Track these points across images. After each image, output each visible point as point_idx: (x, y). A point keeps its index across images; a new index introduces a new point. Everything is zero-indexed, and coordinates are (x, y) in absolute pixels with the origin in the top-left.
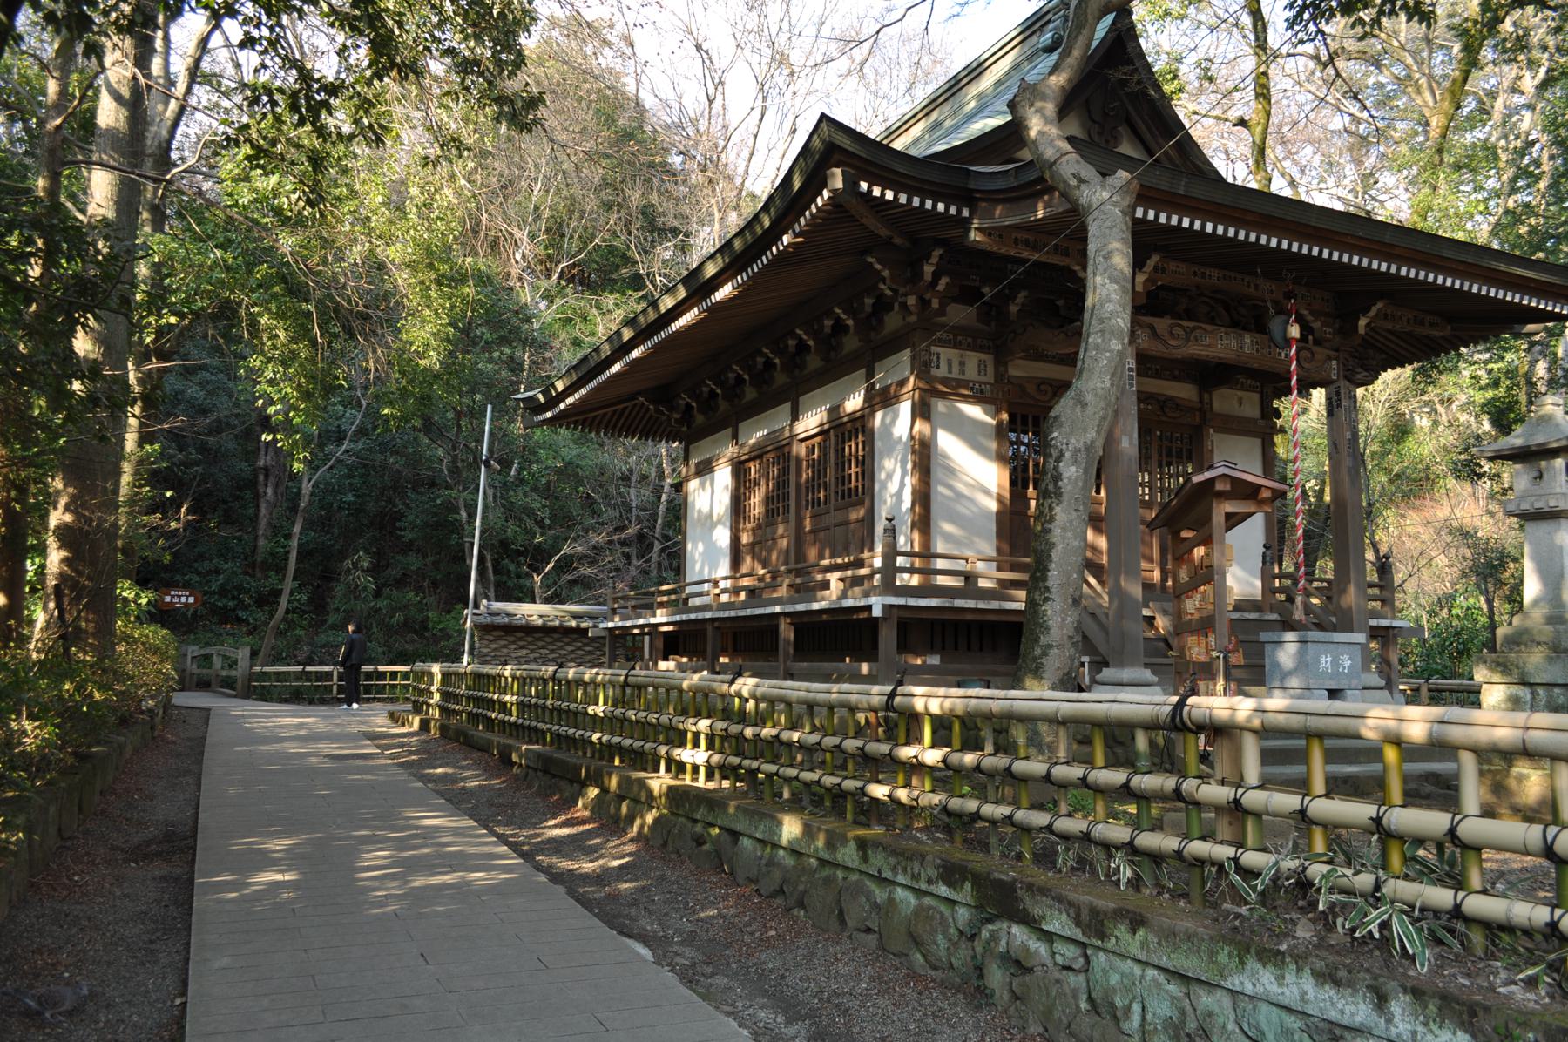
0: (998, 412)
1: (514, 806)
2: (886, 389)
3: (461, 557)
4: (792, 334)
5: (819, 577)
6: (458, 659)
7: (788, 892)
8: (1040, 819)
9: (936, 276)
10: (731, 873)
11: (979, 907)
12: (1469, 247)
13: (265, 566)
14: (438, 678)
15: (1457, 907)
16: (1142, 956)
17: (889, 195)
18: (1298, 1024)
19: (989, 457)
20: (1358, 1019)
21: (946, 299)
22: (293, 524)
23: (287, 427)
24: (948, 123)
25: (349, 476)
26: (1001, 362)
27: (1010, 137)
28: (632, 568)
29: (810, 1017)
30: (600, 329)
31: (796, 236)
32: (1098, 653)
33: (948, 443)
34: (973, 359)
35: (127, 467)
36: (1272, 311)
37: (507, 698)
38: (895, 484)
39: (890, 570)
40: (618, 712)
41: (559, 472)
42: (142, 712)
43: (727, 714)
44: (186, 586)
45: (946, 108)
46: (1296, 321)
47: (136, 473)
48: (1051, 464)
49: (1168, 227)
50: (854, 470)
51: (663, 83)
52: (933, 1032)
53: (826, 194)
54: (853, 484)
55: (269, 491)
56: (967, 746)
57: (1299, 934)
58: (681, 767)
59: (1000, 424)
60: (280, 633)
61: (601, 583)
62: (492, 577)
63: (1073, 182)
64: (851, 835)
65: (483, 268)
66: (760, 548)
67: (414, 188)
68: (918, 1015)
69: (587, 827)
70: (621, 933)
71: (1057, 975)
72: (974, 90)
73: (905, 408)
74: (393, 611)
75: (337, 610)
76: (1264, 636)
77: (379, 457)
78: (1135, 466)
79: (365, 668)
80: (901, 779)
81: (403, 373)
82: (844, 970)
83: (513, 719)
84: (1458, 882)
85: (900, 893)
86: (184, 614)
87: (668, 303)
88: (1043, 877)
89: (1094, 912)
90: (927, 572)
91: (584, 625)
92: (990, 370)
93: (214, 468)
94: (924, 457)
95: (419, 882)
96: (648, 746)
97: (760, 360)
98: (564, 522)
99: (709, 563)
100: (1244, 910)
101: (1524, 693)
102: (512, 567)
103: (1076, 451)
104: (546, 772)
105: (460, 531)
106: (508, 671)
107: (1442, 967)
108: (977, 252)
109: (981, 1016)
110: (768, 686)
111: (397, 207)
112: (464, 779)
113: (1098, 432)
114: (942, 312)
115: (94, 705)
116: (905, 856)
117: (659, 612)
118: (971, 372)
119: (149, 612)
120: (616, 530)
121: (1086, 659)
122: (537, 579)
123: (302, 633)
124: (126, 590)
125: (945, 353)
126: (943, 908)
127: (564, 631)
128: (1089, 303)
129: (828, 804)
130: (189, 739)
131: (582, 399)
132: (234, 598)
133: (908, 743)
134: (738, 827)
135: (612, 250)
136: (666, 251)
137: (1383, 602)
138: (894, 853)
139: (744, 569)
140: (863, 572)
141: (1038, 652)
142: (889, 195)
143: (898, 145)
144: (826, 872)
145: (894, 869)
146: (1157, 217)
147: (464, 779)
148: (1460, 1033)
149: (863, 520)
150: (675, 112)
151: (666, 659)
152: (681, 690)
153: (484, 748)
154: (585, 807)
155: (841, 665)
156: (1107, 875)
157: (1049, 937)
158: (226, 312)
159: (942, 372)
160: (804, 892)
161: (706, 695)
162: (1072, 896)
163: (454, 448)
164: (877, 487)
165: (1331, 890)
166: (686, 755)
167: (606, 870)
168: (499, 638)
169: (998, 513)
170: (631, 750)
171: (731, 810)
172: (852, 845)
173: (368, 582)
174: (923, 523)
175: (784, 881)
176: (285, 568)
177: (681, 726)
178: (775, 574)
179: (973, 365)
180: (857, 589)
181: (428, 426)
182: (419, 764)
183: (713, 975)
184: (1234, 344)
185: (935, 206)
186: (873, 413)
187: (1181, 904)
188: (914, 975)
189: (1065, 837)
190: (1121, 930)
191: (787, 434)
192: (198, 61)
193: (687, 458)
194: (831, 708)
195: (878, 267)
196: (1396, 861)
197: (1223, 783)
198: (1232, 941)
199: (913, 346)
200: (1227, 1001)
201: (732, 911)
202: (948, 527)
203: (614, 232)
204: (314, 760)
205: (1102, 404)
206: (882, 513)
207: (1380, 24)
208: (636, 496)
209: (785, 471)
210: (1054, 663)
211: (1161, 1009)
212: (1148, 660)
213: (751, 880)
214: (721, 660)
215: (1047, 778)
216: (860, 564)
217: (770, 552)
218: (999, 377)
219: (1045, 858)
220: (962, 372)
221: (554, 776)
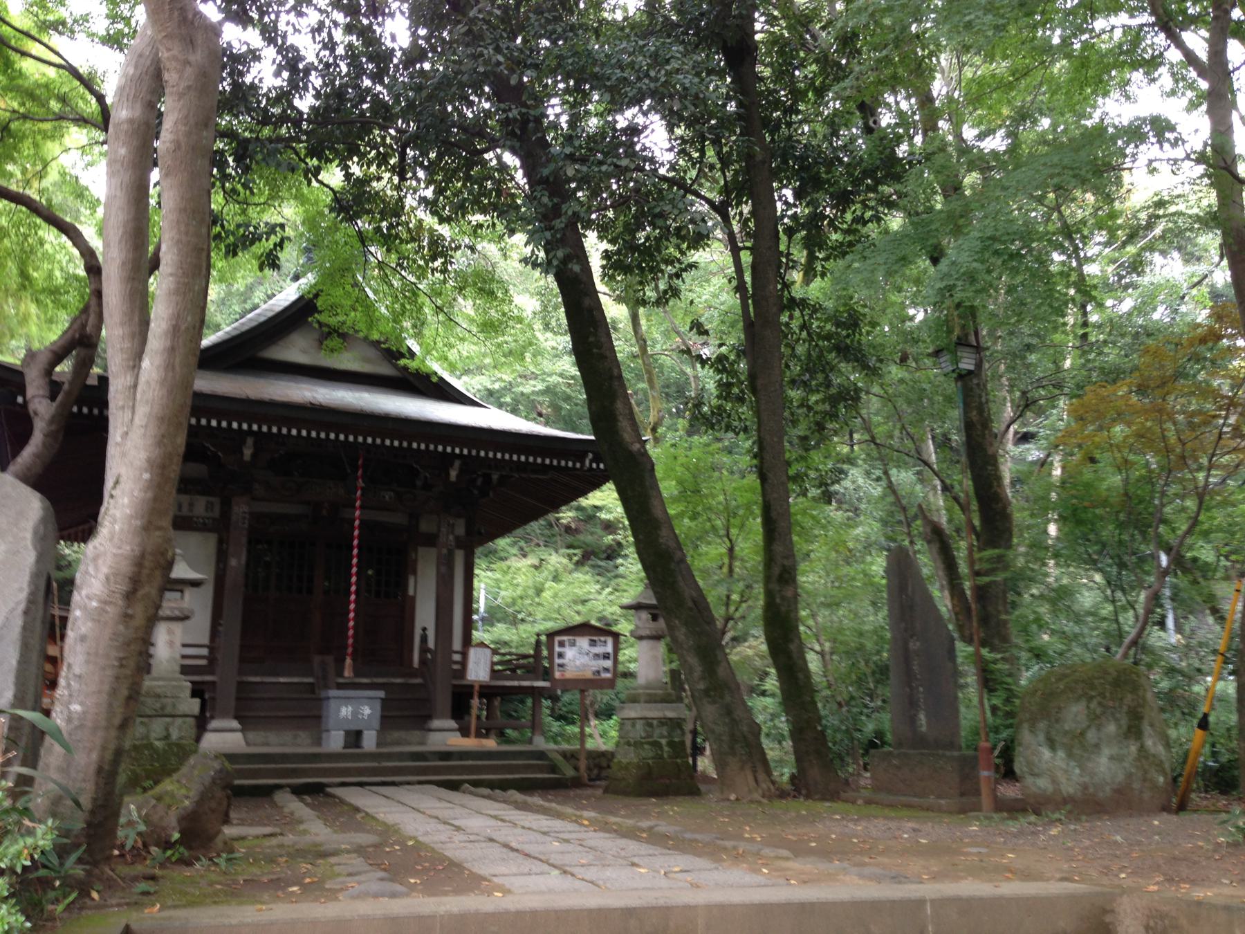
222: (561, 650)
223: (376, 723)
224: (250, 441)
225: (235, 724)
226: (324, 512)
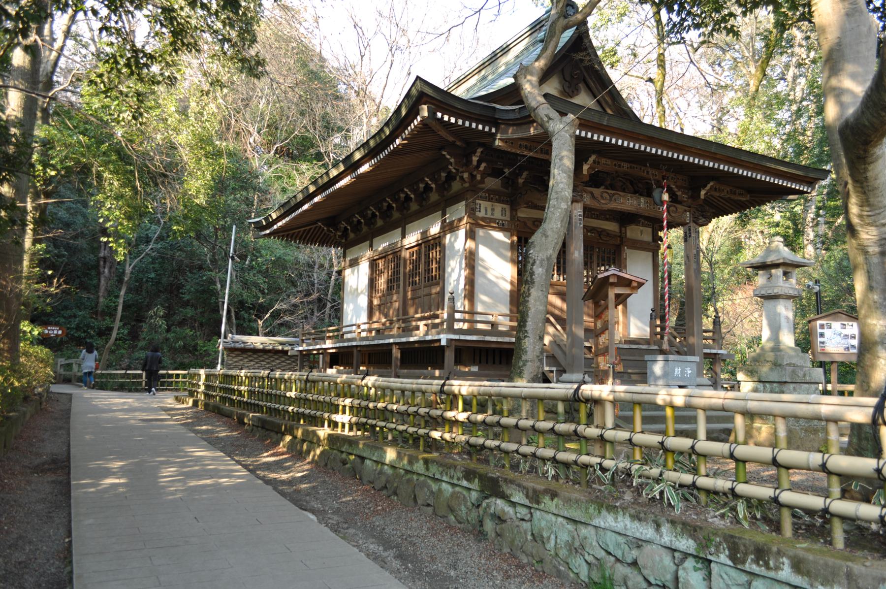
0: (512, 235)
1: (245, 446)
2: (452, 223)
3: (217, 310)
4: (422, 180)
5: (414, 324)
6: (214, 367)
7: (391, 489)
8: (513, 447)
9: (479, 162)
10: (360, 479)
11: (482, 491)
12: (754, 154)
13: (104, 314)
14: (203, 377)
15: (694, 483)
16: (556, 512)
17: (453, 120)
18: (624, 540)
19: (506, 261)
20: (648, 536)
21: (485, 175)
22: (120, 290)
23: (118, 236)
24: (490, 77)
25: (153, 263)
26: (514, 210)
27: (512, 93)
28: (314, 317)
29: (396, 547)
30: (298, 183)
31: (403, 140)
32: (558, 363)
33: (485, 253)
34: (499, 207)
35: (26, 258)
36: (654, 186)
37: (242, 388)
38: (455, 275)
39: (451, 320)
40: (303, 395)
41: (273, 263)
42: (35, 395)
43: (360, 396)
44: (56, 324)
45: (489, 69)
46: (667, 191)
47: (31, 260)
48: (529, 266)
49: (598, 142)
50: (434, 266)
51: (334, 46)
52: (456, 553)
53: (419, 118)
54: (434, 273)
55: (106, 270)
56: (479, 412)
57: (626, 498)
58: (336, 424)
59: (512, 242)
60: (112, 352)
61: (296, 325)
62: (234, 321)
63: (545, 119)
64: (420, 457)
65: (231, 149)
66: (383, 307)
67: (193, 107)
68: (450, 545)
69: (285, 456)
70: (301, 508)
71: (517, 523)
72: (504, 60)
73: (462, 233)
74: (178, 339)
75: (144, 338)
76: (647, 357)
77: (170, 253)
78: (582, 266)
79: (162, 372)
80: (447, 428)
81: (185, 207)
82: (414, 524)
83: (245, 400)
84: (695, 471)
85: (444, 486)
86: (55, 341)
87: (334, 173)
88: (511, 475)
89: (535, 491)
90: (472, 322)
91: (286, 349)
92: (508, 213)
93: (76, 259)
94: (471, 259)
95: (193, 483)
96: (318, 413)
97: (385, 204)
98: (275, 290)
99: (356, 313)
100: (602, 488)
101: (761, 386)
102: (246, 316)
103: (543, 260)
104: (263, 428)
105: (217, 295)
106: (243, 373)
107: (686, 511)
108: (498, 151)
109: (481, 545)
110: (381, 381)
111: (183, 111)
112: (217, 432)
113: (554, 250)
114: (482, 181)
115: (14, 389)
116: (447, 467)
117: (328, 342)
118: (498, 215)
119: (38, 339)
120: (305, 296)
121: (554, 369)
122: (260, 322)
123: (124, 351)
124: (25, 326)
125: (484, 204)
126: (465, 493)
127: (275, 352)
128: (551, 184)
129: (411, 442)
130: (61, 411)
131: (286, 224)
132: (85, 332)
133: (451, 410)
134: (364, 455)
135: (304, 138)
136: (337, 139)
137: (713, 340)
138: (441, 465)
139: (375, 319)
140: (437, 321)
141: (521, 364)
142: (453, 120)
143: (459, 92)
144: (409, 476)
145: (441, 473)
146: (592, 136)
147: (217, 432)
148: (690, 540)
149: (439, 293)
150: (342, 61)
151: (331, 367)
152: (336, 383)
153: (229, 416)
154: (284, 446)
155: (425, 371)
156: (543, 474)
157: (514, 504)
158: (86, 170)
159: (481, 214)
160: (397, 487)
161: (350, 386)
162: (525, 484)
163: (214, 249)
164: (446, 275)
165: (640, 477)
166: (338, 418)
167: (294, 478)
168: (238, 356)
169: (511, 292)
170: (310, 416)
171: (361, 446)
172: (421, 462)
173: (161, 323)
174: (470, 295)
175: (387, 481)
176: (115, 315)
177: (336, 403)
178: (391, 322)
179: (499, 211)
180: (434, 331)
181: (198, 236)
182: (192, 424)
183: (347, 528)
184: (635, 202)
185: (477, 126)
186: (445, 235)
187: (576, 486)
188: (450, 527)
189: (525, 456)
190: (547, 499)
191: (399, 245)
192: (69, 28)
193: (344, 257)
194: (413, 392)
195: (448, 157)
196: (670, 463)
197: (597, 427)
198: (596, 502)
199: (467, 200)
200: (592, 531)
201: (360, 498)
202: (484, 298)
203: (306, 128)
204: (132, 422)
205: (556, 236)
206: (449, 288)
207: (713, 35)
208: (317, 276)
209: (398, 266)
210: (529, 369)
211: (564, 537)
212: (587, 370)
213: (370, 482)
214: (361, 368)
215: (517, 426)
216: (437, 317)
217: (389, 310)
218: (513, 217)
219: (515, 467)
220: (493, 214)
221: (267, 430)
222: (822, 331)
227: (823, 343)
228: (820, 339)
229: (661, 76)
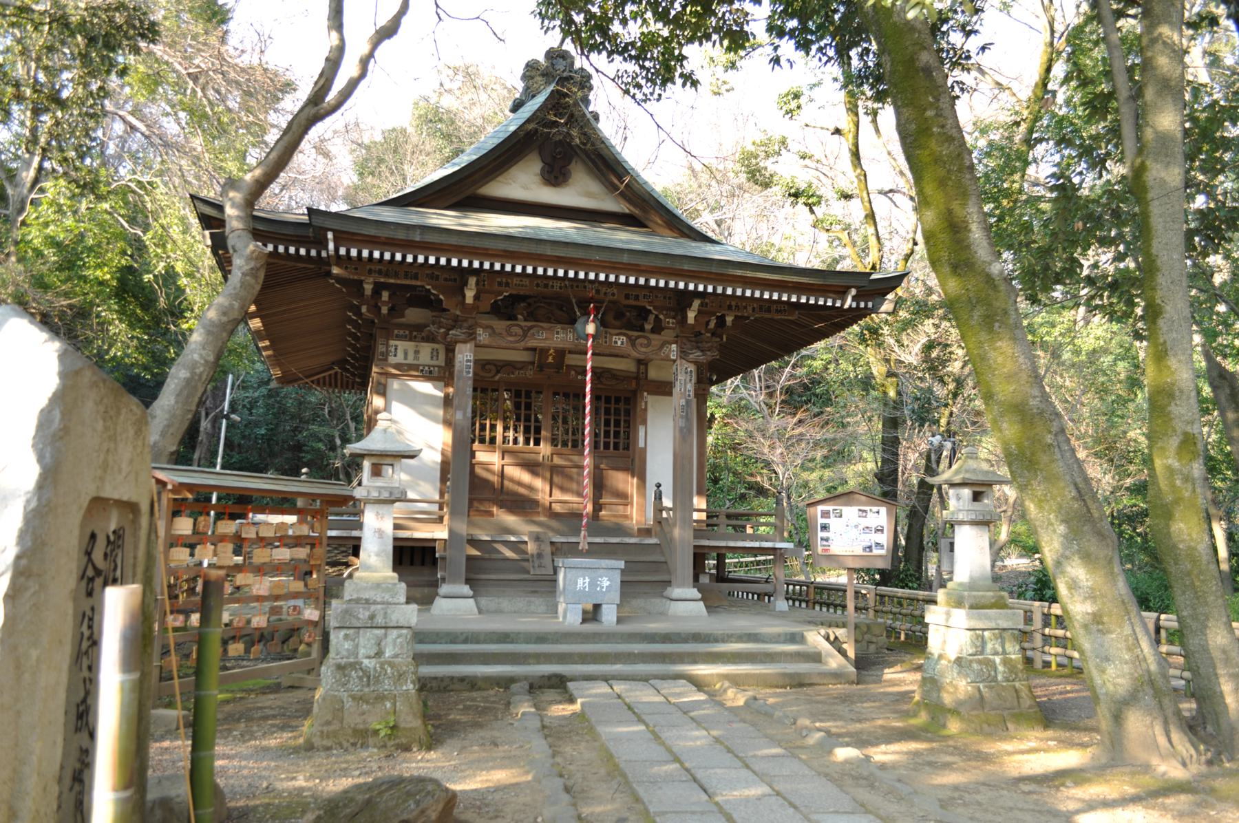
59: (447, 397)
92: (442, 356)
222: (825, 521)
223: (616, 596)
224: (472, 281)
225: (466, 589)
226: (550, 360)
227: (827, 540)
228: (821, 534)
229: (852, 125)
